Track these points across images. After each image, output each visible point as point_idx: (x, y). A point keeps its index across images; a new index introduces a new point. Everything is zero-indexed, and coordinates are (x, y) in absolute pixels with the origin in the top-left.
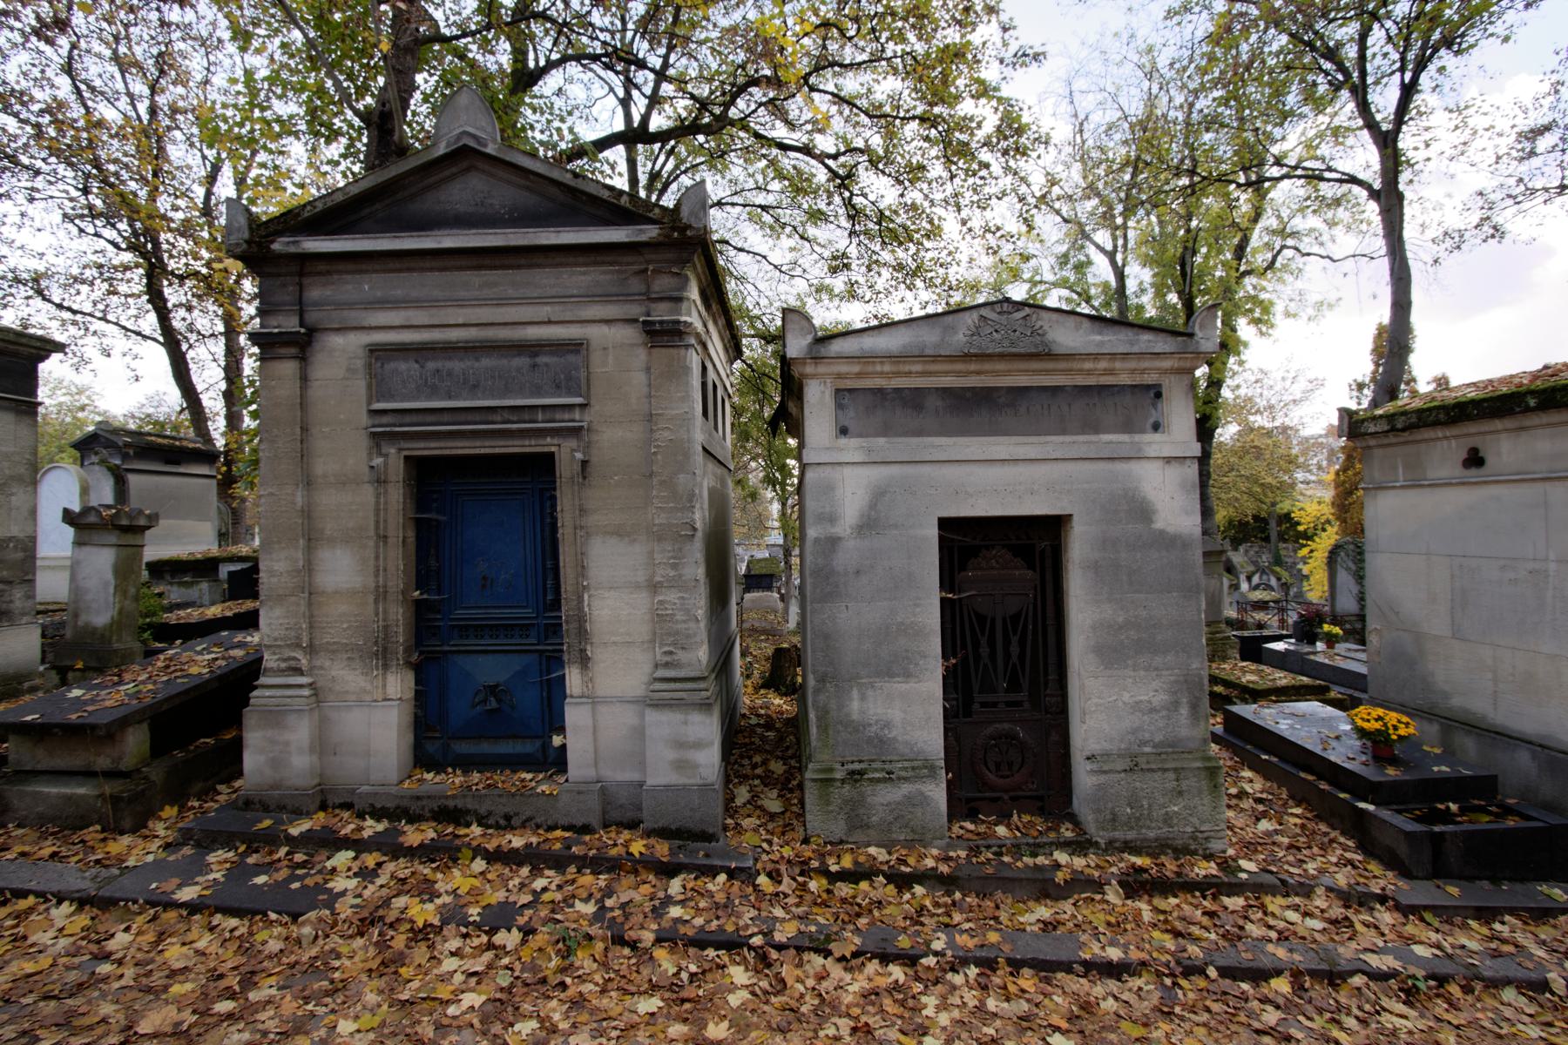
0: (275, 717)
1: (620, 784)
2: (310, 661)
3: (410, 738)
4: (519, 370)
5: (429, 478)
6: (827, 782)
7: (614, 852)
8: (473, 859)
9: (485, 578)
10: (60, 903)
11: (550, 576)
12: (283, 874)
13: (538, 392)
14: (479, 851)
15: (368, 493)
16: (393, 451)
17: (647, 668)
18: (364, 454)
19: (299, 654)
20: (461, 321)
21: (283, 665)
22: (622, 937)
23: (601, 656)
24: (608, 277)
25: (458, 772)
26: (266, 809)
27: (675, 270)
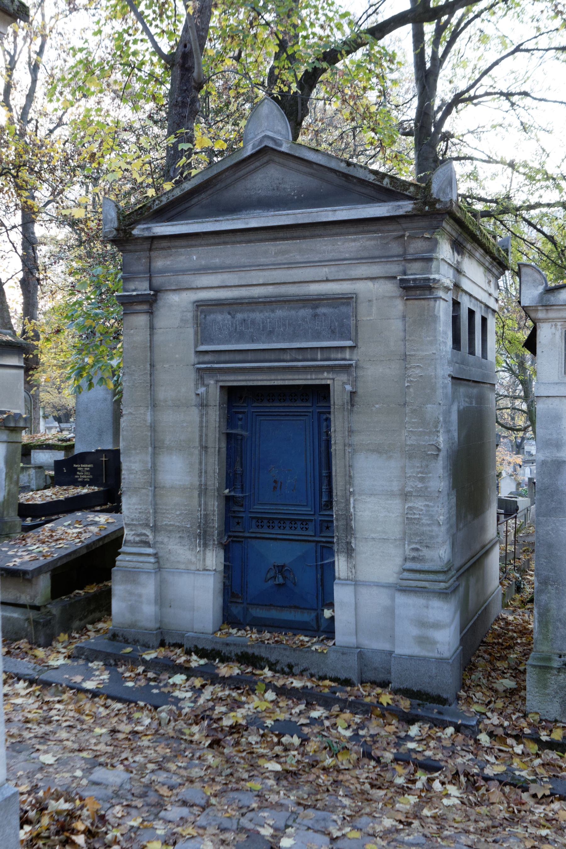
0: (132, 575)
1: (374, 651)
2: (154, 537)
3: (220, 600)
4: (303, 319)
5: (236, 398)
6: (545, 669)
7: (368, 700)
8: (265, 691)
9: (275, 482)
10: (19, 679)
11: (325, 482)
12: (143, 683)
13: (317, 336)
14: (269, 686)
15: (195, 413)
16: (212, 382)
17: (399, 561)
18: (192, 385)
19: (148, 532)
20: (261, 282)
21: (137, 539)
22: (370, 754)
23: (363, 549)
24: (373, 242)
25: (255, 630)
26: (127, 642)
27: (427, 235)
